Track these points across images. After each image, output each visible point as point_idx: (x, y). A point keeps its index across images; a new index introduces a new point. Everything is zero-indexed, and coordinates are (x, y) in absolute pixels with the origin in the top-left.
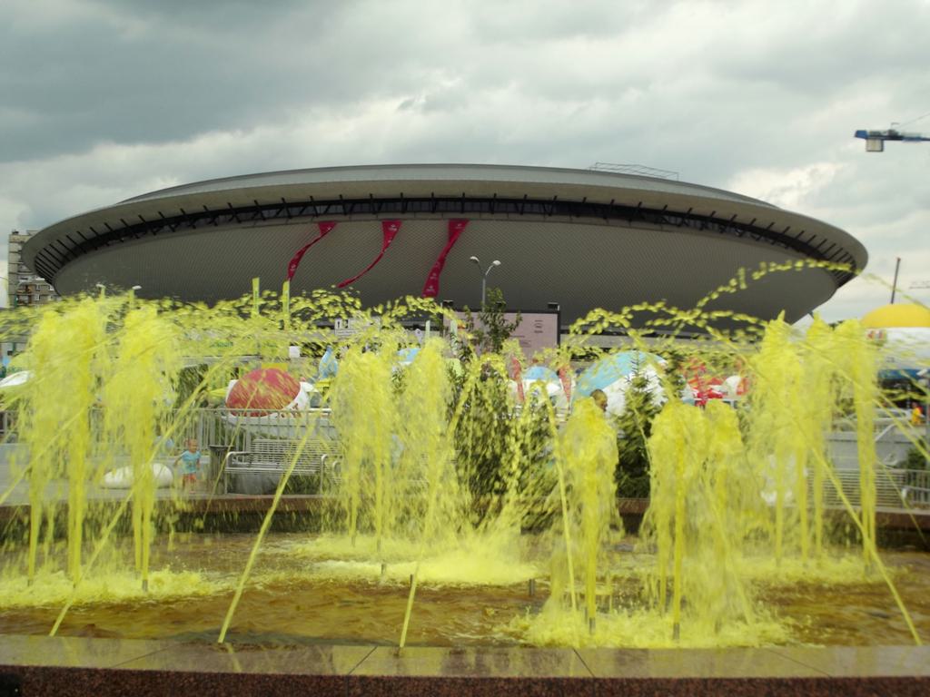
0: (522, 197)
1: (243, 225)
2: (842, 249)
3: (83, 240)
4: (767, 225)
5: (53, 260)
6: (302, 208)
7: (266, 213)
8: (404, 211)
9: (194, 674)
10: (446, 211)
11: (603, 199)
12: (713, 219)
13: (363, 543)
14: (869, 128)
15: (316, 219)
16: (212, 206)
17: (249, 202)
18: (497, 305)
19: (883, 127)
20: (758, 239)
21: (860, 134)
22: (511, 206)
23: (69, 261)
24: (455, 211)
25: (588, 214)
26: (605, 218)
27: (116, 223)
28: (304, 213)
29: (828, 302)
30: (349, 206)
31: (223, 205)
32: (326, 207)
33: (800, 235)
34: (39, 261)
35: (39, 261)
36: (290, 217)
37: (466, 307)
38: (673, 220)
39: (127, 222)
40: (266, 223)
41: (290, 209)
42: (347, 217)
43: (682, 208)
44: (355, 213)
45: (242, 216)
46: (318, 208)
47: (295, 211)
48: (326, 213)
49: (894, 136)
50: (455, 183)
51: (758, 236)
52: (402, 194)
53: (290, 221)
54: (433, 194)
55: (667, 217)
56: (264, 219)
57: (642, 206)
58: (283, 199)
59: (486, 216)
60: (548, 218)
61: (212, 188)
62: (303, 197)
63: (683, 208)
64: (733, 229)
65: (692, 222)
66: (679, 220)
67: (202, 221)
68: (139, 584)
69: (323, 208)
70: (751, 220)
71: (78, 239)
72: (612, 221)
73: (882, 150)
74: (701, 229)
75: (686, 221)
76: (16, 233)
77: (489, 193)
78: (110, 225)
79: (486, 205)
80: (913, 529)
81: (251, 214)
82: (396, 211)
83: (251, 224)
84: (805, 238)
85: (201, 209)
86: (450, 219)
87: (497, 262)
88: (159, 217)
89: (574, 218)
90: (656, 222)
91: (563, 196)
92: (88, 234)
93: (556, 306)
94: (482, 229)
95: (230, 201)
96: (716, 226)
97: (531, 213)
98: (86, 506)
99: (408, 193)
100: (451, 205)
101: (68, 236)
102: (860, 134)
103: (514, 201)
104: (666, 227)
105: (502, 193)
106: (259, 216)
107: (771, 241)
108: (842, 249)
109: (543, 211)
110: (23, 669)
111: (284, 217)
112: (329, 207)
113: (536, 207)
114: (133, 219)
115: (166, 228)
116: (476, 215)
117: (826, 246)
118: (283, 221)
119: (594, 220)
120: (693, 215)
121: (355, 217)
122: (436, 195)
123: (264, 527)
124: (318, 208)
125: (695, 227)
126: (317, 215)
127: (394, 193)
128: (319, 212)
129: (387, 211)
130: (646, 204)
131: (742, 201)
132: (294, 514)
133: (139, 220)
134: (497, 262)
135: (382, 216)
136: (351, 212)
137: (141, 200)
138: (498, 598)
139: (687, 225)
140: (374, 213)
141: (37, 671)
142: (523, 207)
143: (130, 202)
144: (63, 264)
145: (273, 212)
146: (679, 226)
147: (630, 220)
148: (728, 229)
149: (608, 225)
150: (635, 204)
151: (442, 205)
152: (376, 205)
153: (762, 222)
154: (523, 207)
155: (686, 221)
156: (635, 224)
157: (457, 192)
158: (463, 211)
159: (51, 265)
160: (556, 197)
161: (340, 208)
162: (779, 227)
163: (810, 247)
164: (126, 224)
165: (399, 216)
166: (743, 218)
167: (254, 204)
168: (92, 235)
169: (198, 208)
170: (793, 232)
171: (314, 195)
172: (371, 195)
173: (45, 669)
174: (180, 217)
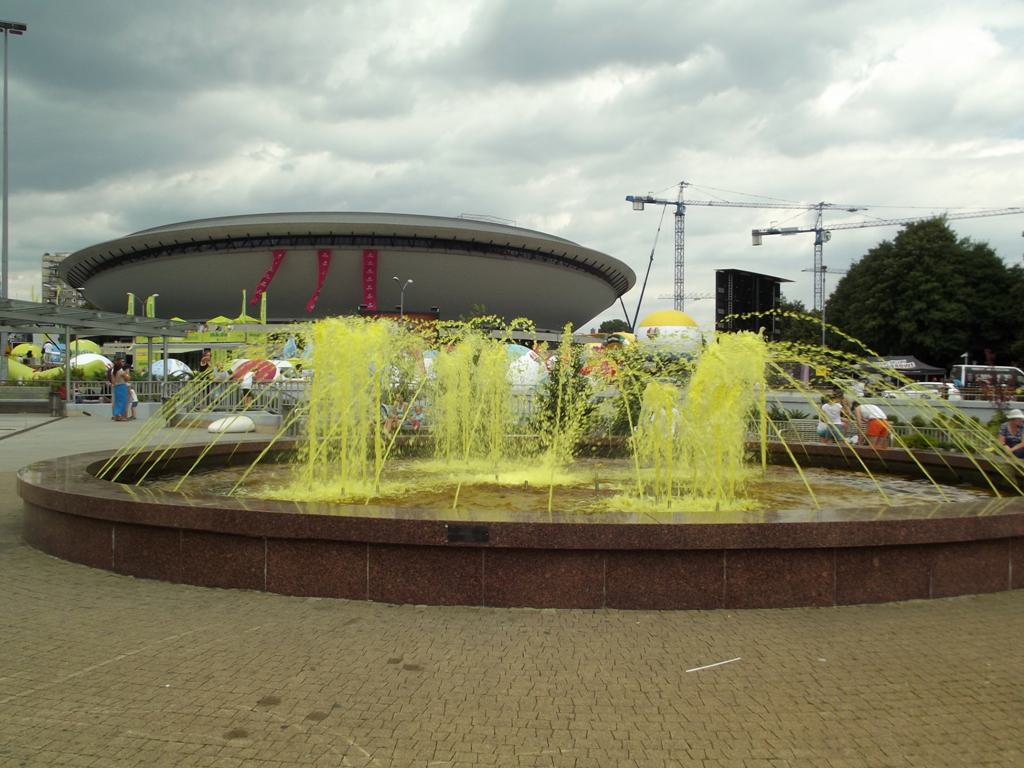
0: (413, 235)
1: (220, 251)
5: (83, 269)
7: (235, 244)
8: (333, 244)
9: (582, 525)
10: (362, 244)
11: (467, 238)
13: (454, 464)
14: (635, 195)
15: (272, 248)
16: (198, 238)
17: (223, 235)
18: (428, 309)
19: (643, 194)
21: (629, 198)
22: (240, 243)
23: (93, 275)
24: (367, 244)
27: (128, 249)
30: (294, 240)
31: (205, 237)
36: (253, 246)
37: (461, 316)
42: (293, 247)
45: (219, 245)
47: (256, 242)
48: (278, 244)
49: (650, 201)
53: (254, 249)
56: (234, 248)
59: (388, 247)
60: (430, 250)
61: (194, 226)
62: (262, 233)
66: (517, 253)
67: (190, 248)
68: (500, 478)
71: (100, 260)
73: (643, 209)
76: (47, 254)
77: (390, 233)
80: (841, 457)
81: (225, 245)
82: (326, 244)
83: (225, 251)
84: (597, 266)
85: (190, 240)
86: (364, 250)
87: (410, 281)
89: (448, 251)
90: (501, 254)
91: (441, 236)
92: (108, 256)
94: (389, 257)
97: (420, 246)
99: (335, 231)
100: (365, 240)
102: (629, 198)
103: (426, 239)
105: (400, 233)
110: (489, 524)
113: (423, 242)
114: (140, 247)
115: (165, 253)
116: (382, 247)
117: (611, 271)
118: (248, 249)
119: (461, 252)
121: (298, 247)
122: (355, 233)
123: (254, 464)
126: (272, 245)
127: (326, 231)
129: (321, 244)
130: (495, 242)
133: (145, 248)
134: (410, 281)
135: (317, 247)
136: (296, 244)
140: (312, 244)
141: (497, 524)
144: (88, 277)
146: (517, 256)
150: (488, 242)
151: (376, 240)
152: (313, 240)
153: (570, 255)
156: (488, 255)
157: (368, 231)
158: (373, 245)
161: (288, 241)
165: (329, 247)
166: (559, 252)
169: (187, 239)
170: (590, 262)
173: (502, 523)
174: (175, 245)
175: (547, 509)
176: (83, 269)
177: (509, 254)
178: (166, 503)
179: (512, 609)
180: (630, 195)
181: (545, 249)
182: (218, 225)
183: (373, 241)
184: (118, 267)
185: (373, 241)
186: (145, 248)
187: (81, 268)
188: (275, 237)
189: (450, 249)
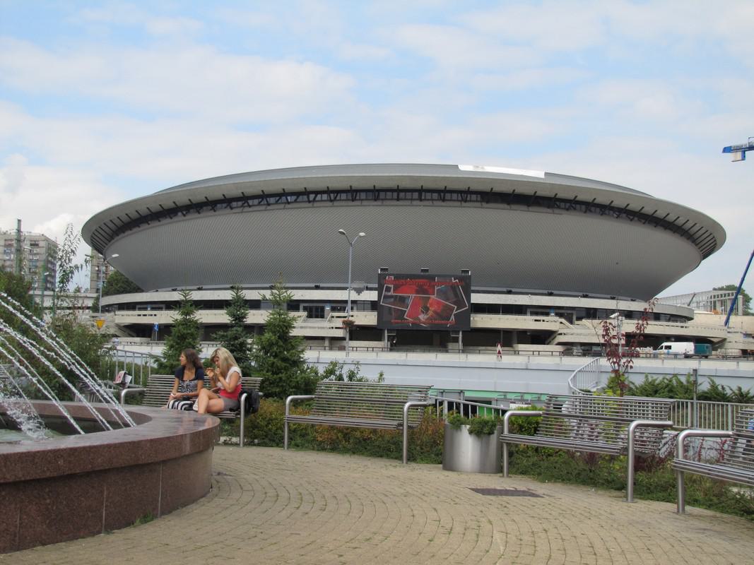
0: (443, 188)
4: (609, 203)
5: (104, 233)
6: (277, 198)
7: (250, 202)
12: (627, 210)
20: (631, 220)
22: (435, 195)
25: (496, 201)
26: (509, 204)
28: (280, 201)
32: (295, 197)
33: (641, 209)
34: (95, 237)
35: (95, 237)
38: (562, 205)
39: (177, 204)
40: (251, 209)
41: (268, 199)
43: (570, 195)
44: (317, 201)
46: (289, 198)
47: (272, 200)
50: (522, 176)
51: (631, 217)
52: (351, 187)
53: (269, 208)
55: (558, 203)
56: (250, 206)
57: (537, 194)
58: (284, 190)
63: (570, 196)
64: (611, 212)
65: (578, 206)
69: (294, 198)
70: (592, 199)
72: (513, 207)
74: (585, 212)
75: (574, 205)
78: (130, 215)
79: (416, 195)
87: (362, 234)
88: (173, 205)
93: (468, 271)
96: (598, 210)
100: (389, 194)
101: (111, 221)
104: (557, 211)
106: (246, 204)
107: (643, 221)
109: (460, 198)
111: (264, 205)
112: (298, 197)
113: (455, 196)
120: (613, 207)
124: (289, 198)
125: (581, 210)
128: (289, 200)
130: (540, 193)
131: (625, 192)
134: (362, 234)
137: (176, 190)
139: (575, 209)
142: (444, 195)
143: (164, 192)
144: (112, 238)
145: (256, 201)
146: (567, 210)
147: (529, 206)
148: (607, 212)
149: (510, 209)
150: (532, 193)
151: (382, 195)
153: (634, 206)
154: (444, 195)
155: (574, 205)
160: (469, 188)
161: (325, 197)
162: (648, 210)
163: (683, 230)
166: (619, 203)
167: (241, 195)
168: (128, 220)
171: (244, 191)
172: (374, 186)
174: (189, 205)
175: (388, 333)
176: (104, 233)
177: (559, 207)
178: (655, 366)
179: (726, 369)
180: (727, 145)
181: (601, 200)
182: (207, 185)
183: (420, 196)
184: (135, 230)
185: (420, 196)
186: (189, 203)
187: (101, 231)
188: (292, 194)
189: (487, 202)
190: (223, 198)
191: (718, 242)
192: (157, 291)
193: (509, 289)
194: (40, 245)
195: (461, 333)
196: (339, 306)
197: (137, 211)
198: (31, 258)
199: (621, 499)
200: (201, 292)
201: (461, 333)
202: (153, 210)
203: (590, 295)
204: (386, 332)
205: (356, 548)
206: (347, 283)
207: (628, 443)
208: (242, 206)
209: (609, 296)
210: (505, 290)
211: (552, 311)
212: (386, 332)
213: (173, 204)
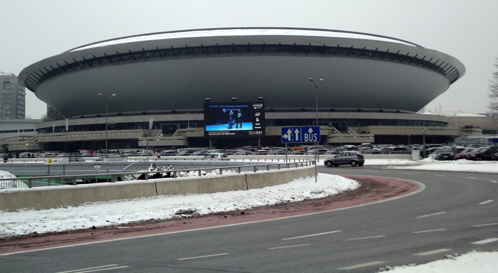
2: (451, 66)
3: (47, 72)
29: (20, 71)
34: (28, 81)
35: (28, 81)
54: (217, 44)
55: (364, 52)
70: (407, 53)
71: (44, 71)
84: (427, 59)
85: (103, 55)
88: (73, 62)
95: (130, 49)
98: (193, 210)
108: (451, 66)
128: (148, 56)
130: (341, 46)
132: (67, 130)
138: (307, 206)
139: (375, 56)
144: (41, 82)
159: (35, 83)
164: (67, 64)
175: (212, 141)
190: (116, 53)
191: (460, 73)
192: (72, 118)
193: (380, 109)
194: (11, 82)
195: (259, 140)
196: (184, 124)
197: (65, 61)
198: (4, 92)
199: (217, 216)
200: (83, 119)
201: (259, 140)
202: (69, 63)
203: (384, 110)
204: (210, 141)
205: (11, 223)
206: (318, 107)
207: (173, 177)
208: (119, 60)
209: (95, 115)
210: (356, 109)
211: (330, 122)
212: (210, 141)
213: (65, 63)
